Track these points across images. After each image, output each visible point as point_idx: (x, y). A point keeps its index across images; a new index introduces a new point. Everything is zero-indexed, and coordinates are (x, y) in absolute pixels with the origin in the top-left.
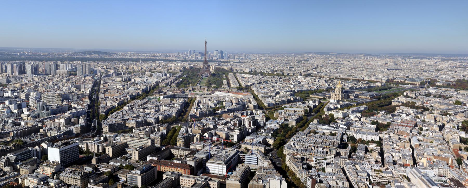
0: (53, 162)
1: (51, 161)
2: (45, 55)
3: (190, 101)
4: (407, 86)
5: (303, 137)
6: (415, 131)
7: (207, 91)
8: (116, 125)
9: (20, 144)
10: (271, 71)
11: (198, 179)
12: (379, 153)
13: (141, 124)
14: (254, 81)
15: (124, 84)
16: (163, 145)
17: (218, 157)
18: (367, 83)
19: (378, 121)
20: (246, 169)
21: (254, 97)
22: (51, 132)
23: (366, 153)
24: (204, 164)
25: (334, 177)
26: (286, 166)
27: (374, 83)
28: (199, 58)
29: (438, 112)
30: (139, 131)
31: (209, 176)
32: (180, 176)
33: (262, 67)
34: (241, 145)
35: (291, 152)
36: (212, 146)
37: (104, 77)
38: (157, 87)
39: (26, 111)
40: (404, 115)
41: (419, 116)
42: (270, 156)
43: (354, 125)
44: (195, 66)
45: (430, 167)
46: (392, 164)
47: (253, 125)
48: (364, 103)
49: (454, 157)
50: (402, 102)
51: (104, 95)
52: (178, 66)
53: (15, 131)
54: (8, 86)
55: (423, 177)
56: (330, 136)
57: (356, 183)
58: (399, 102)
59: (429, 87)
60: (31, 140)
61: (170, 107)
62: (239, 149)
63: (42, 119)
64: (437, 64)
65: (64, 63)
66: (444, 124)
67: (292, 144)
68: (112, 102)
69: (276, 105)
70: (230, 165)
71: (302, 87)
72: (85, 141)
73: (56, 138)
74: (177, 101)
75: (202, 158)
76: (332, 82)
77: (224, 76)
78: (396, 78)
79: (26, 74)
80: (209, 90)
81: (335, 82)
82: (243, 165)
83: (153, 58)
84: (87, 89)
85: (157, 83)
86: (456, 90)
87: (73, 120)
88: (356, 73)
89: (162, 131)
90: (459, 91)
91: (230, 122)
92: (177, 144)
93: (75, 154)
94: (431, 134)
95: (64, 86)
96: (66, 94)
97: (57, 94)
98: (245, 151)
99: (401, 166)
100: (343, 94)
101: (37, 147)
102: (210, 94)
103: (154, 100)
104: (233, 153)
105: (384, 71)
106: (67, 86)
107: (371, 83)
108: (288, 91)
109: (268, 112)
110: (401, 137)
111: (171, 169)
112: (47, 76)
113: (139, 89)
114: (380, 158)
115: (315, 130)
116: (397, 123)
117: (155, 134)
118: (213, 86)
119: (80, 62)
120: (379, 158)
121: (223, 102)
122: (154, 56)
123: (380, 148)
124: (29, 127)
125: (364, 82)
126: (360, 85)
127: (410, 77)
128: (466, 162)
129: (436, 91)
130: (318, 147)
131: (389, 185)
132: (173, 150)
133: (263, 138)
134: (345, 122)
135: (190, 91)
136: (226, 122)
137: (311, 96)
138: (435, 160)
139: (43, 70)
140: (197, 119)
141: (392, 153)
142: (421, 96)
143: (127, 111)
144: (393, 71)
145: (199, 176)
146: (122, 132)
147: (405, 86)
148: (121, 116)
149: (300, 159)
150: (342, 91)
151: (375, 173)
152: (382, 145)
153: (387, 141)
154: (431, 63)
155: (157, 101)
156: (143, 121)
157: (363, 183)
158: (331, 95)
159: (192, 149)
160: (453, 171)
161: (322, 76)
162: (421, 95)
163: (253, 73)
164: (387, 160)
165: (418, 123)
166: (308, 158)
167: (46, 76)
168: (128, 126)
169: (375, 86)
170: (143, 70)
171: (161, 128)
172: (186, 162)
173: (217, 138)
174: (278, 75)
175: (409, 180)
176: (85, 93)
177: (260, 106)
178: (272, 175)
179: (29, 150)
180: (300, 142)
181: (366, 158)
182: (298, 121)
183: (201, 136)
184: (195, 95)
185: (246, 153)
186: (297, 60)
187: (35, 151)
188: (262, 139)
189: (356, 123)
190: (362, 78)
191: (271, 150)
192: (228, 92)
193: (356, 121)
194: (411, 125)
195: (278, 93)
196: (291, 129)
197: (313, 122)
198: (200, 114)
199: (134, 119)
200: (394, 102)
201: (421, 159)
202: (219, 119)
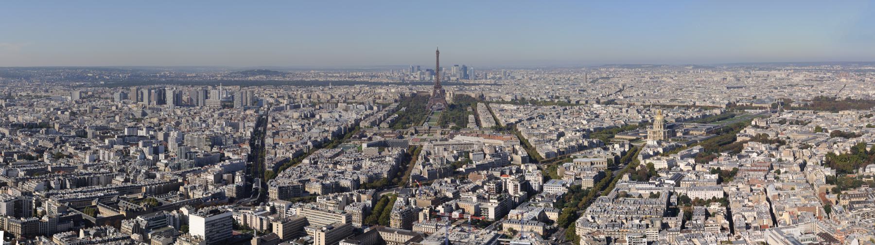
0: (195, 236)
1: (192, 235)
2: (192, 77)
3: (413, 152)
6: (771, 177)
7: (442, 134)
8: (289, 189)
9: (153, 205)
10: (549, 98)
13: (330, 188)
14: (521, 115)
15: (303, 123)
16: (367, 225)
18: (700, 111)
19: (720, 167)
21: (522, 143)
22: (195, 191)
23: (706, 219)
27: (710, 109)
28: (427, 78)
29: (796, 144)
30: (327, 200)
33: (534, 92)
34: (502, 224)
35: (588, 231)
36: (451, 228)
37: (274, 111)
38: (357, 127)
39: (164, 159)
40: (755, 155)
41: (774, 153)
42: (554, 239)
43: (686, 179)
44: (419, 92)
45: (794, 223)
46: (745, 229)
47: (521, 190)
48: (698, 142)
49: (821, 204)
50: (751, 137)
51: (272, 140)
52: (391, 93)
53: (149, 185)
54: (143, 121)
56: (650, 199)
58: (746, 136)
59: (783, 111)
60: (167, 201)
61: (378, 161)
62: (498, 231)
63: (183, 171)
64: (790, 77)
65: (216, 89)
66: (805, 160)
67: (589, 218)
69: (560, 155)
71: (601, 122)
72: (242, 211)
73: (201, 202)
74: (389, 151)
76: (648, 112)
77: (470, 109)
78: (739, 101)
79: (166, 104)
81: (653, 112)
83: (350, 79)
84: (248, 130)
85: (357, 122)
86: (815, 112)
87: (225, 176)
88: (683, 96)
89: (365, 201)
90: (818, 113)
91: (482, 187)
92: (390, 223)
93: (227, 228)
94: (791, 178)
96: (218, 136)
97: (205, 136)
98: (509, 234)
99: (757, 230)
100: (666, 130)
101: (175, 212)
102: (446, 140)
103: (352, 150)
104: (488, 238)
105: (722, 90)
107: (706, 110)
108: (578, 131)
109: (546, 167)
110: (753, 188)
112: (193, 108)
114: (728, 222)
115: (626, 192)
116: (746, 168)
117: (353, 205)
118: (450, 126)
119: (239, 87)
120: (726, 224)
123: (725, 208)
124: (166, 183)
125: (696, 110)
126: (692, 114)
127: (758, 98)
128: (835, 208)
129: (790, 115)
130: (632, 219)
132: (383, 233)
133: (540, 211)
134: (672, 175)
135: (412, 134)
136: (474, 187)
137: (616, 136)
138: (799, 213)
139: (188, 98)
140: (425, 182)
141: (743, 213)
142: (774, 124)
143: (308, 167)
144: (735, 90)
146: (299, 201)
147: (752, 111)
148: (298, 175)
149: (604, 240)
152: (728, 203)
153: (734, 197)
154: (782, 75)
155: (356, 152)
156: (333, 185)
158: (648, 133)
159: (416, 232)
160: (822, 224)
161: (632, 103)
162: (774, 123)
163: (518, 101)
164: (737, 224)
165: (773, 164)
167: (191, 108)
168: (308, 190)
169: (712, 115)
170: (334, 100)
173: (460, 213)
174: (561, 104)
176: (244, 135)
177: (533, 158)
179: (165, 215)
180: (602, 213)
181: (708, 226)
182: (597, 179)
183: (431, 211)
184: (420, 141)
185: (511, 238)
186: (590, 79)
187: (172, 218)
188: (539, 212)
189: (689, 175)
190: (692, 103)
191: (555, 230)
192: (478, 136)
193: (688, 171)
194: (765, 168)
195: (561, 135)
196: (586, 192)
197: (621, 179)
198: (429, 174)
199: (319, 181)
200: (739, 136)
201: (781, 215)
202: (462, 182)
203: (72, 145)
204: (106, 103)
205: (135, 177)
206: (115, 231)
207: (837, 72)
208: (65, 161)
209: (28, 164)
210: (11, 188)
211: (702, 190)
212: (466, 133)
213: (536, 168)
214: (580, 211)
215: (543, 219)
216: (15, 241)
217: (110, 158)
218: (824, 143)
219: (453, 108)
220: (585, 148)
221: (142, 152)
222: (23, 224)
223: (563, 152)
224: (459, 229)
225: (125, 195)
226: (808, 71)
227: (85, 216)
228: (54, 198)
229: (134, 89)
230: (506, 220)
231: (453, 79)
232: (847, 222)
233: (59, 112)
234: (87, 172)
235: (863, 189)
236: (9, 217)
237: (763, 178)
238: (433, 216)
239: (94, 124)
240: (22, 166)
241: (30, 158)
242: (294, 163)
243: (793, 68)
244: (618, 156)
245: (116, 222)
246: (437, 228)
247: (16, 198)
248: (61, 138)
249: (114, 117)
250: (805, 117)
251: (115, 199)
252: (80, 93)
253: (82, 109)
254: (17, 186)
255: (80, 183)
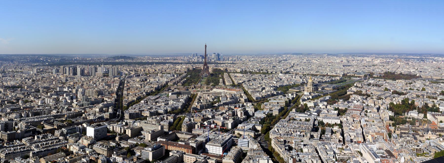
0: (89, 137)
2: (89, 60)
3: (193, 96)
4: (356, 78)
5: (285, 123)
6: (363, 114)
7: (207, 88)
10: (258, 70)
11: (199, 157)
12: (341, 133)
13: (153, 114)
14: (244, 79)
15: (141, 84)
17: (215, 141)
18: (330, 78)
20: (239, 150)
21: (245, 93)
22: (90, 116)
23: (332, 134)
24: (204, 146)
25: (310, 156)
26: (272, 148)
28: (201, 60)
30: (152, 119)
31: (208, 156)
32: (184, 154)
33: (251, 67)
36: (210, 132)
37: (128, 78)
39: (75, 101)
40: (355, 101)
41: (365, 101)
42: (259, 140)
43: (322, 112)
47: (244, 115)
50: (354, 92)
52: (183, 68)
53: (68, 114)
54: (66, 84)
55: (370, 152)
57: (326, 160)
58: (352, 91)
60: (77, 121)
62: (233, 134)
64: (373, 61)
66: (380, 106)
67: (276, 130)
68: (132, 97)
69: (263, 98)
70: (226, 147)
72: (112, 124)
73: (93, 121)
74: (182, 97)
75: (202, 141)
76: (305, 78)
77: (220, 76)
79: (77, 75)
80: (208, 88)
81: (307, 78)
82: (236, 147)
83: (164, 61)
85: (167, 83)
87: (104, 109)
88: (322, 70)
91: (225, 113)
94: (372, 116)
95: (100, 85)
99: (356, 143)
100: (314, 87)
101: (80, 126)
102: (209, 91)
103: (164, 96)
104: (228, 138)
106: (102, 85)
107: (333, 77)
108: (272, 87)
109: (256, 104)
110: (354, 119)
111: (176, 148)
113: (153, 87)
114: (342, 137)
116: (351, 108)
118: (211, 84)
119: (111, 65)
120: (341, 138)
121: (219, 97)
122: (165, 60)
125: (328, 77)
126: (326, 79)
127: (357, 71)
129: (373, 81)
130: (296, 132)
131: (349, 161)
132: (178, 134)
135: (193, 88)
136: (222, 113)
137: (290, 90)
145: (200, 155)
149: (283, 142)
150: (313, 85)
151: (339, 151)
152: (343, 127)
153: (345, 124)
157: (331, 161)
158: (305, 88)
160: (387, 144)
161: (298, 73)
164: (346, 139)
166: (289, 141)
168: (143, 115)
170: (156, 72)
171: (169, 118)
172: (189, 144)
174: (264, 73)
175: (361, 154)
177: (250, 100)
178: (261, 156)
180: (282, 128)
181: (332, 139)
182: (280, 111)
183: (201, 124)
184: (196, 92)
185: (239, 138)
190: (326, 74)
191: (260, 135)
192: (224, 89)
193: (324, 108)
195: (264, 89)
196: (275, 117)
198: (200, 107)
200: (348, 91)
201: (368, 136)
202: (216, 111)
203: (33, 96)
204: (49, 75)
205: (62, 110)
206: (52, 136)
207: (396, 58)
208: (29, 104)
209: (12, 106)
210: (3, 117)
211: (330, 119)
212: (218, 88)
213: (251, 105)
214: (272, 126)
215: (254, 129)
216: (4, 143)
217: (50, 102)
218: (389, 97)
219: (212, 76)
220: (274, 95)
221: (65, 99)
222: (8, 134)
223: (264, 97)
224: (214, 133)
225: (57, 119)
226: (382, 58)
227: (38, 129)
228: (23, 122)
229: (62, 67)
230: (237, 129)
231: (213, 60)
232: (399, 145)
233: (27, 80)
234: (39, 109)
235: (407, 125)
236: (2, 131)
237: (359, 114)
238: (202, 126)
239: (43, 86)
240: (9, 107)
241: (13, 103)
242: (137, 102)
243: (375, 56)
244: (290, 100)
245: (52, 132)
246: (204, 132)
247: (6, 122)
248: (27, 93)
249: (53, 82)
250: (380, 82)
251: (52, 121)
252: (37, 69)
253: (38, 78)
254: (6, 116)
255: (36, 114)
